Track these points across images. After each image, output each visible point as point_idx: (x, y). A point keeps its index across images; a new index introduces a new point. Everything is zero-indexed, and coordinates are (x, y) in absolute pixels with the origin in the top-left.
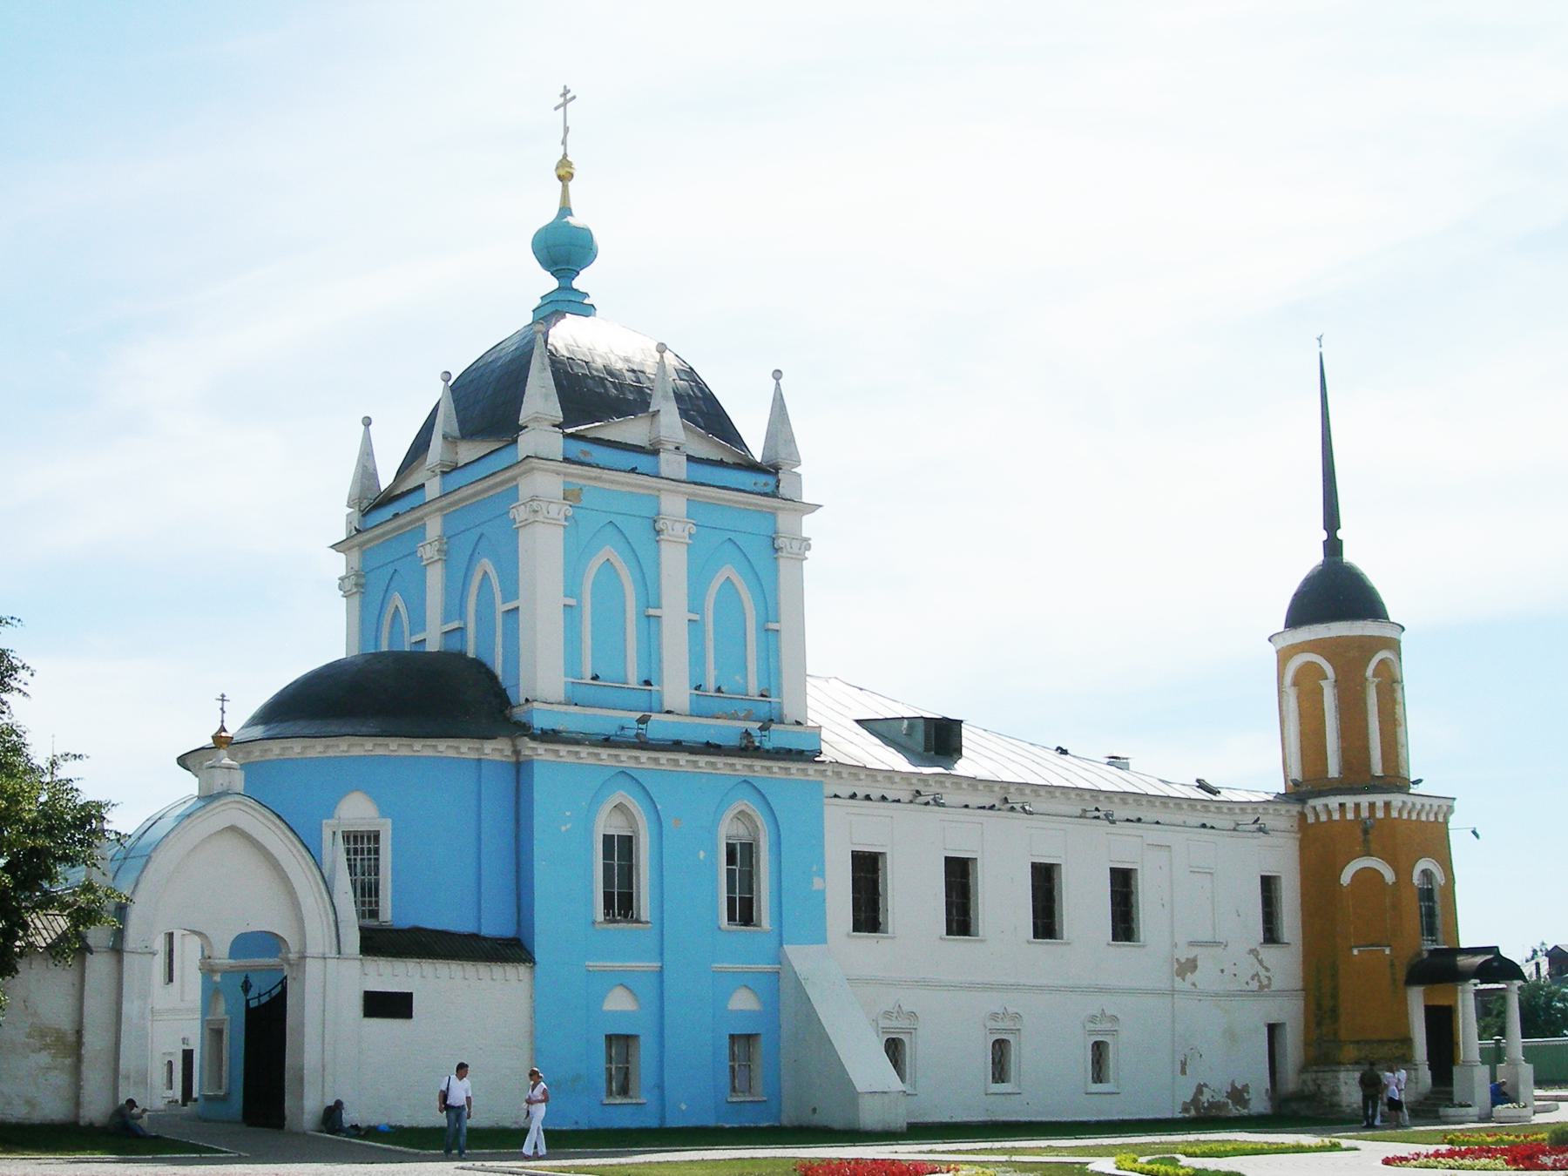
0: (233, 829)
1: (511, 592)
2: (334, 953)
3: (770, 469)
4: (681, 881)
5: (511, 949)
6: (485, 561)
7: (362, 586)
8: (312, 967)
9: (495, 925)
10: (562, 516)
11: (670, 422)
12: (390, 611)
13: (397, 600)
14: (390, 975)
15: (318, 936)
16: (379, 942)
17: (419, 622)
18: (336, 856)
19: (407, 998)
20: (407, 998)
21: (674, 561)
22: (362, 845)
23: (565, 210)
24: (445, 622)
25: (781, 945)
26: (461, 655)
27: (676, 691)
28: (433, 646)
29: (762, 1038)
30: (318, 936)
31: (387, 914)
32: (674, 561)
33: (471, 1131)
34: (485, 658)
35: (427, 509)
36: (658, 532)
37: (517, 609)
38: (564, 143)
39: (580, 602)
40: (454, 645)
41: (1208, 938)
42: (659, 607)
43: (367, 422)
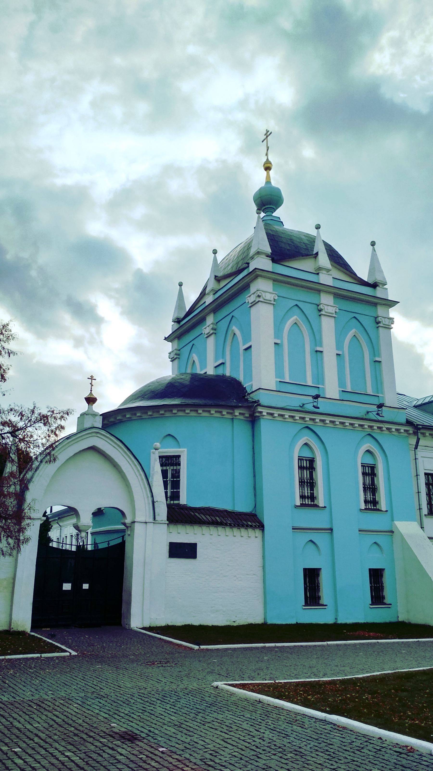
0: (93, 449)
1: (247, 336)
2: (151, 520)
3: (374, 286)
4: (341, 486)
5: (249, 521)
6: (234, 328)
7: (215, 330)
8: (138, 529)
9: (242, 506)
10: (272, 299)
11: (324, 260)
12: (190, 362)
13: (195, 357)
14: (184, 535)
15: (142, 512)
16: (179, 515)
17: (204, 364)
18: (156, 469)
19: (194, 546)
20: (194, 546)
21: (328, 326)
22: (170, 462)
23: (268, 182)
24: (216, 360)
25: (393, 520)
26: (224, 376)
27: (332, 389)
28: (210, 371)
29: (386, 570)
30: (142, 512)
31: (183, 500)
32: (328, 326)
33: (34, 627)
34: (234, 376)
35: (206, 311)
36: (378, 323)
37: (250, 347)
38: (267, 155)
39: (282, 341)
40: (220, 372)
41: (155, 500)
42: (321, 346)
43: (181, 285)
